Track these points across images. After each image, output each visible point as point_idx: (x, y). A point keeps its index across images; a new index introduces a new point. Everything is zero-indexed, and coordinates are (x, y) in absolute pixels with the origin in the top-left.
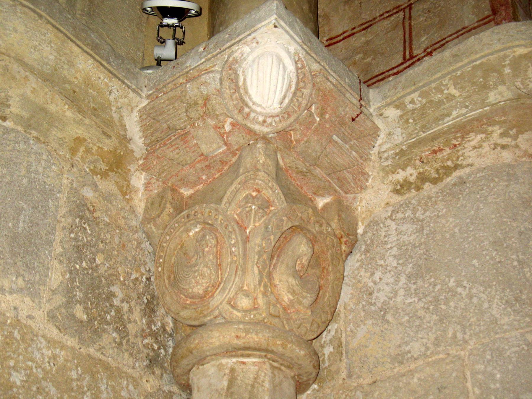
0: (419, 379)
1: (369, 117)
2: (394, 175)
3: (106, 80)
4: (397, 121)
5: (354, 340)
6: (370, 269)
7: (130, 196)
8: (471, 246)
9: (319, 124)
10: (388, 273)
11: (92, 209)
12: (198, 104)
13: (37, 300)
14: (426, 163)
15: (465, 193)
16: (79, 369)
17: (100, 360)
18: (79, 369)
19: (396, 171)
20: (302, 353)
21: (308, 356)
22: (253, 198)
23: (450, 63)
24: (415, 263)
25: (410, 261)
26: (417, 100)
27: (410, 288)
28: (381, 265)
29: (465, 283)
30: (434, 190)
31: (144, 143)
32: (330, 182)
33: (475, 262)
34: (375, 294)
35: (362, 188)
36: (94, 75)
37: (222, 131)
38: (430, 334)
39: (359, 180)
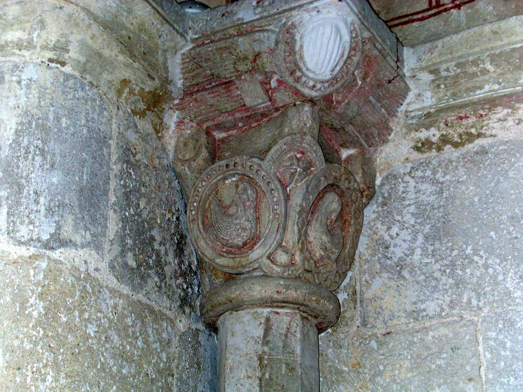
0: (433, 337)
1: (403, 77)
2: (417, 133)
3: (158, 25)
4: (428, 84)
5: (369, 291)
6: (386, 223)
7: (162, 133)
8: (490, 218)
9: (360, 88)
10: (405, 230)
11: (134, 151)
12: (248, 59)
13: (100, 252)
14: (450, 127)
15: (487, 163)
16: (133, 315)
17: (147, 305)
18: (133, 315)
19: (419, 129)
20: (331, 307)
21: (335, 310)
22: (298, 160)
23: (489, 40)
24: (433, 224)
25: (428, 222)
26: (452, 69)
27: (427, 249)
28: (398, 221)
29: (482, 253)
30: (456, 154)
31: (183, 85)
32: (358, 137)
33: (492, 234)
34: (391, 249)
35: (384, 141)
36: (149, 21)
37: (268, 87)
38: (445, 296)
39: (383, 134)
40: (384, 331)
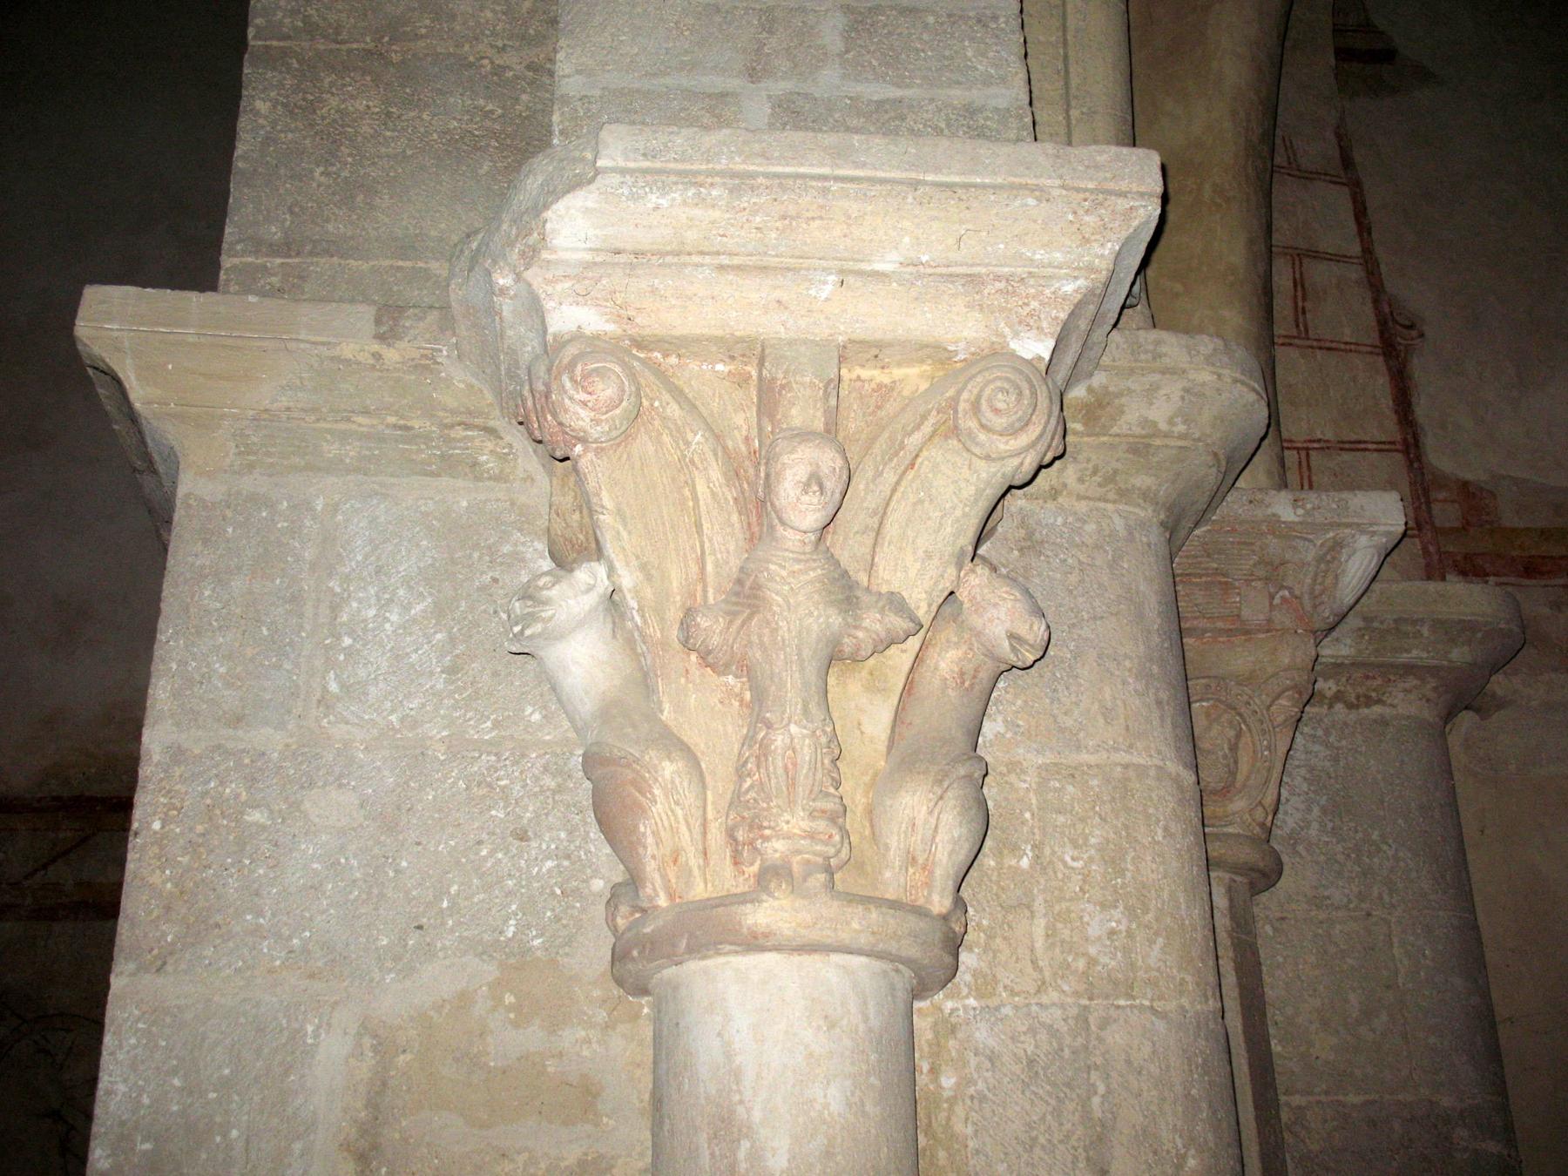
40: (1278, 915)
